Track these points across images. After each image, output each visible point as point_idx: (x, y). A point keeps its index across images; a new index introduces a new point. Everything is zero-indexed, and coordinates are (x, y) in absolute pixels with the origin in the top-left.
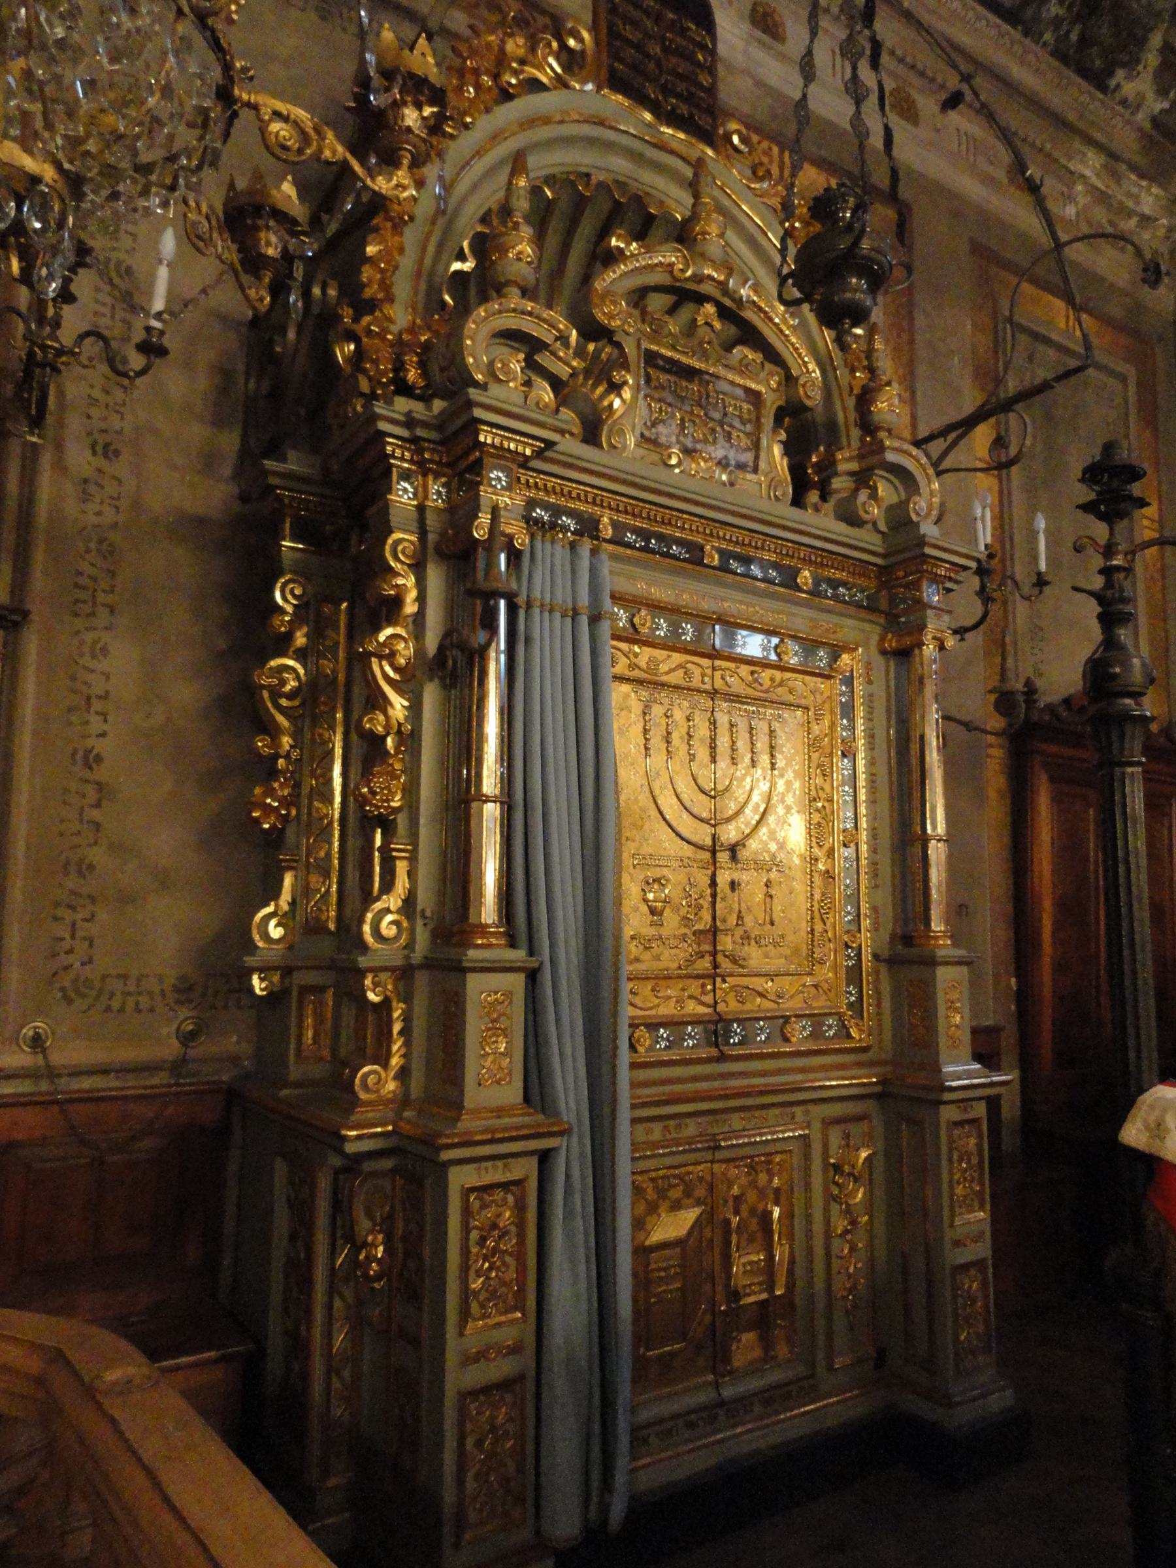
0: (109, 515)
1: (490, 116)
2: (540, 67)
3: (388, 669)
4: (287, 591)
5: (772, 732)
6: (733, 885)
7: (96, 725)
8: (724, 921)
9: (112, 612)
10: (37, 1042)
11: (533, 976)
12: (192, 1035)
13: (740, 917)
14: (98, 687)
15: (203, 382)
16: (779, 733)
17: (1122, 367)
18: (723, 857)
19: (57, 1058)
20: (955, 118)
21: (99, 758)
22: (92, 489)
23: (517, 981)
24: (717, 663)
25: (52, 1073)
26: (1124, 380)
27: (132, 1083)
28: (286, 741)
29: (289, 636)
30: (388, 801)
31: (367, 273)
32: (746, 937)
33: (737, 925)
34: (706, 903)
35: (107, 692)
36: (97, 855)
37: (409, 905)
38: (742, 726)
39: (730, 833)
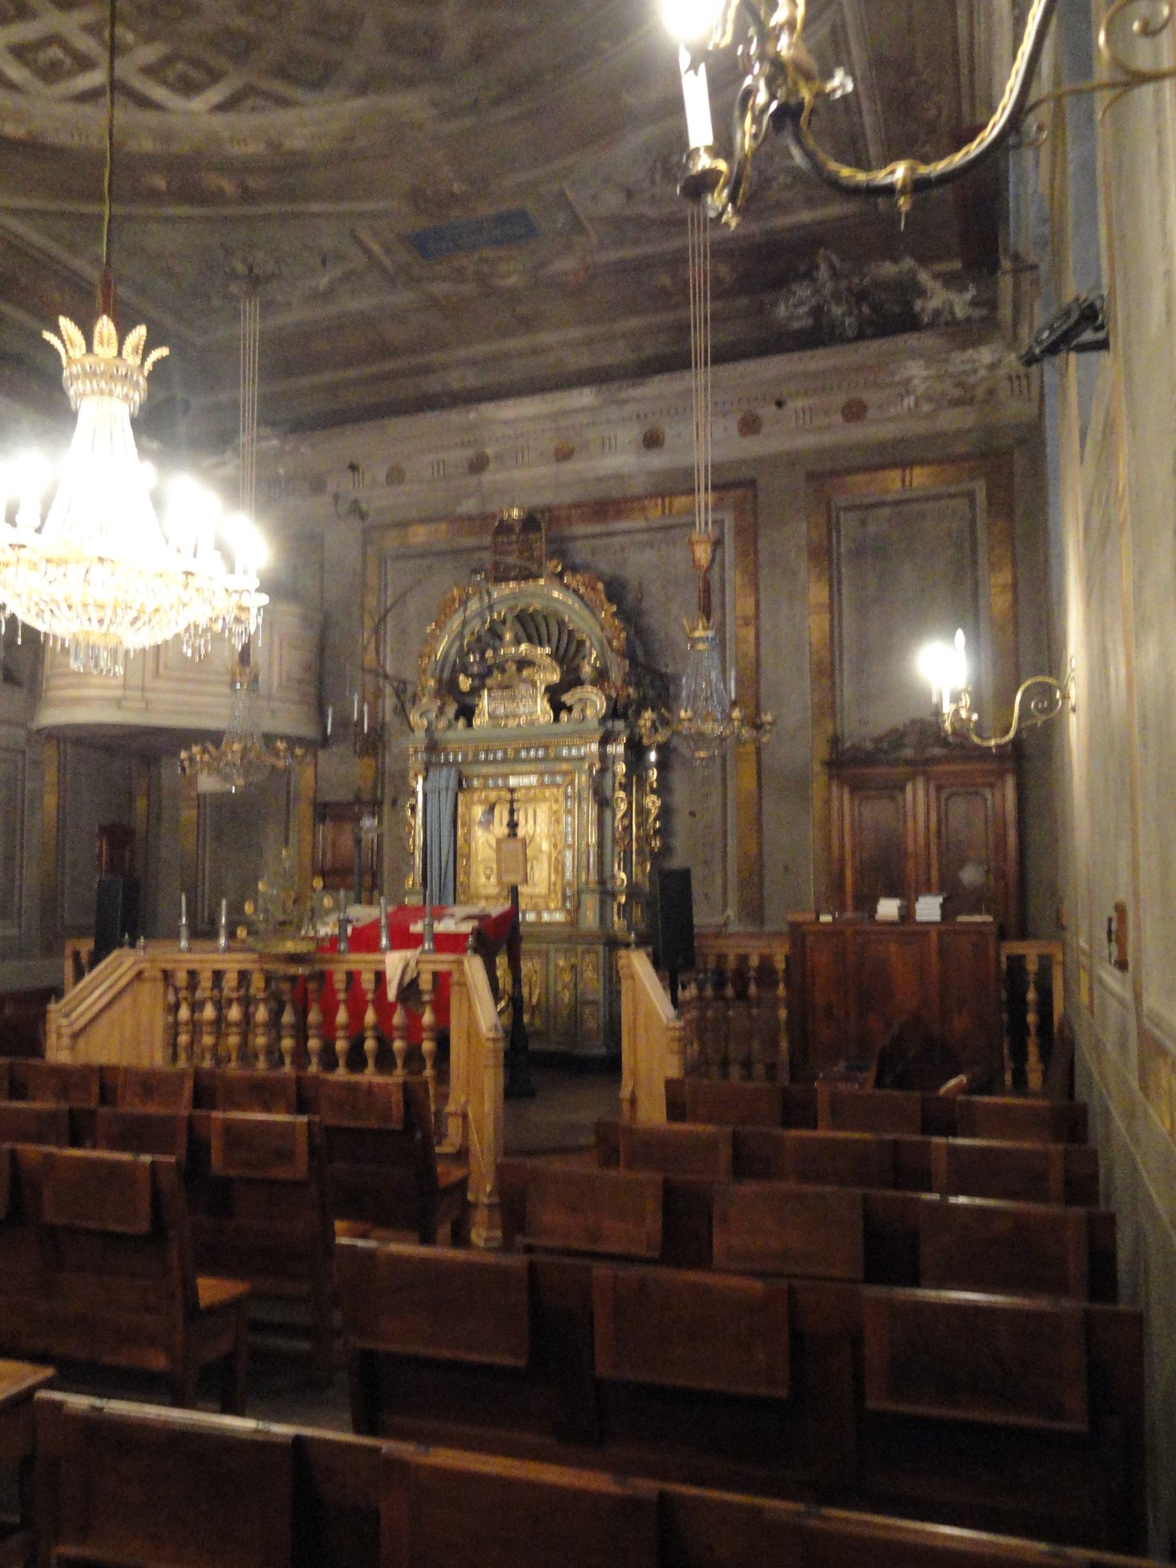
17: (965, 486)
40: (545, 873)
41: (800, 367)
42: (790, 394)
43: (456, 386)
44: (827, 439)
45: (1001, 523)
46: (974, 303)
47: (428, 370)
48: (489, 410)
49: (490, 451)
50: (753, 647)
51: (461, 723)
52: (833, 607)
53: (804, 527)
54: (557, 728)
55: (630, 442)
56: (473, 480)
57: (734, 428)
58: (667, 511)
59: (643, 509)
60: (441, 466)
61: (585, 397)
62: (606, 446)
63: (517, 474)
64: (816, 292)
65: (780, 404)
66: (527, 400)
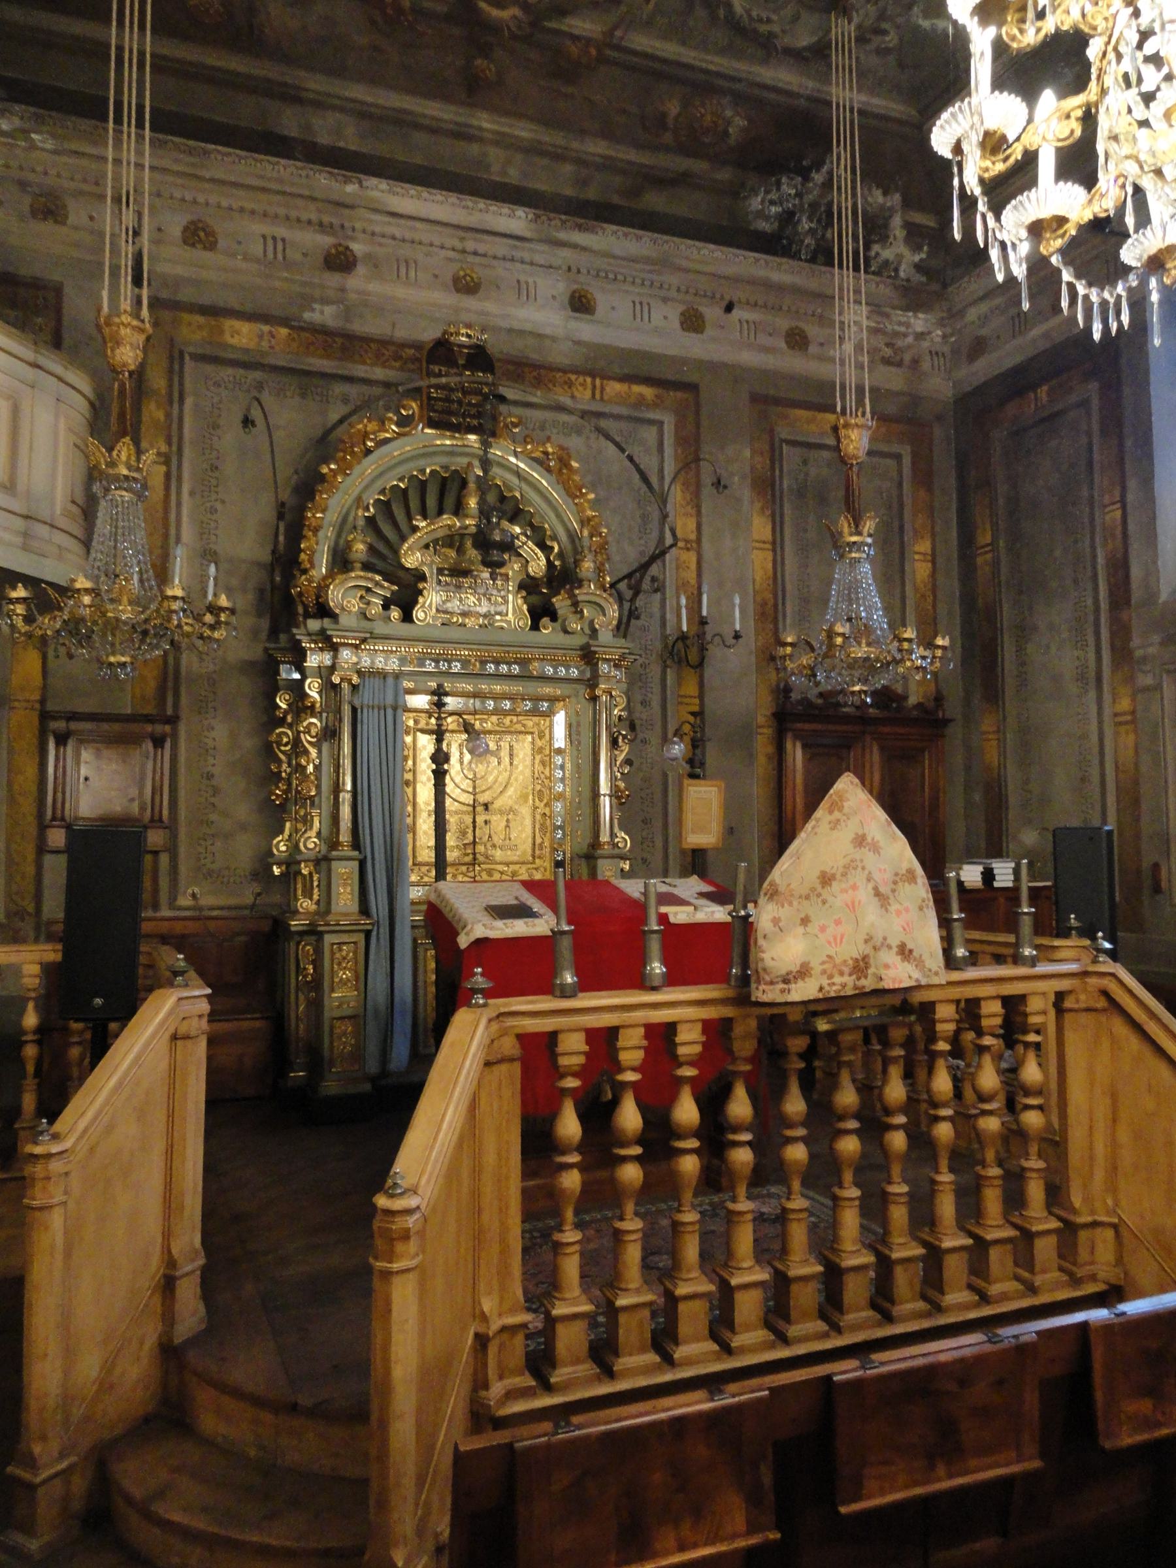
0: (211, 667)
2: (387, 431)
3: (309, 738)
5: (511, 747)
6: (486, 822)
7: (211, 761)
10: (194, 895)
12: (259, 894)
13: (490, 836)
14: (211, 743)
15: (250, 596)
17: (895, 448)
18: (479, 809)
19: (203, 902)
20: (737, 313)
21: (213, 776)
22: (204, 657)
23: (356, 864)
25: (201, 909)
26: (898, 457)
27: (234, 913)
28: (285, 766)
29: (284, 718)
31: (303, 556)
32: (494, 846)
34: (470, 831)
36: (213, 817)
37: (319, 835)
39: (483, 798)
41: (761, 272)
43: (324, 139)
44: (770, 362)
45: (922, 493)
46: (918, 267)
47: (293, 96)
48: (378, 189)
49: (357, 248)
50: (694, 575)
51: (395, 613)
52: (776, 545)
53: (747, 453)
54: (534, 637)
56: (333, 280)
58: (598, 396)
59: (570, 384)
61: (516, 220)
62: (523, 292)
63: (401, 292)
64: (799, 195)
65: (729, 308)
66: (439, 196)
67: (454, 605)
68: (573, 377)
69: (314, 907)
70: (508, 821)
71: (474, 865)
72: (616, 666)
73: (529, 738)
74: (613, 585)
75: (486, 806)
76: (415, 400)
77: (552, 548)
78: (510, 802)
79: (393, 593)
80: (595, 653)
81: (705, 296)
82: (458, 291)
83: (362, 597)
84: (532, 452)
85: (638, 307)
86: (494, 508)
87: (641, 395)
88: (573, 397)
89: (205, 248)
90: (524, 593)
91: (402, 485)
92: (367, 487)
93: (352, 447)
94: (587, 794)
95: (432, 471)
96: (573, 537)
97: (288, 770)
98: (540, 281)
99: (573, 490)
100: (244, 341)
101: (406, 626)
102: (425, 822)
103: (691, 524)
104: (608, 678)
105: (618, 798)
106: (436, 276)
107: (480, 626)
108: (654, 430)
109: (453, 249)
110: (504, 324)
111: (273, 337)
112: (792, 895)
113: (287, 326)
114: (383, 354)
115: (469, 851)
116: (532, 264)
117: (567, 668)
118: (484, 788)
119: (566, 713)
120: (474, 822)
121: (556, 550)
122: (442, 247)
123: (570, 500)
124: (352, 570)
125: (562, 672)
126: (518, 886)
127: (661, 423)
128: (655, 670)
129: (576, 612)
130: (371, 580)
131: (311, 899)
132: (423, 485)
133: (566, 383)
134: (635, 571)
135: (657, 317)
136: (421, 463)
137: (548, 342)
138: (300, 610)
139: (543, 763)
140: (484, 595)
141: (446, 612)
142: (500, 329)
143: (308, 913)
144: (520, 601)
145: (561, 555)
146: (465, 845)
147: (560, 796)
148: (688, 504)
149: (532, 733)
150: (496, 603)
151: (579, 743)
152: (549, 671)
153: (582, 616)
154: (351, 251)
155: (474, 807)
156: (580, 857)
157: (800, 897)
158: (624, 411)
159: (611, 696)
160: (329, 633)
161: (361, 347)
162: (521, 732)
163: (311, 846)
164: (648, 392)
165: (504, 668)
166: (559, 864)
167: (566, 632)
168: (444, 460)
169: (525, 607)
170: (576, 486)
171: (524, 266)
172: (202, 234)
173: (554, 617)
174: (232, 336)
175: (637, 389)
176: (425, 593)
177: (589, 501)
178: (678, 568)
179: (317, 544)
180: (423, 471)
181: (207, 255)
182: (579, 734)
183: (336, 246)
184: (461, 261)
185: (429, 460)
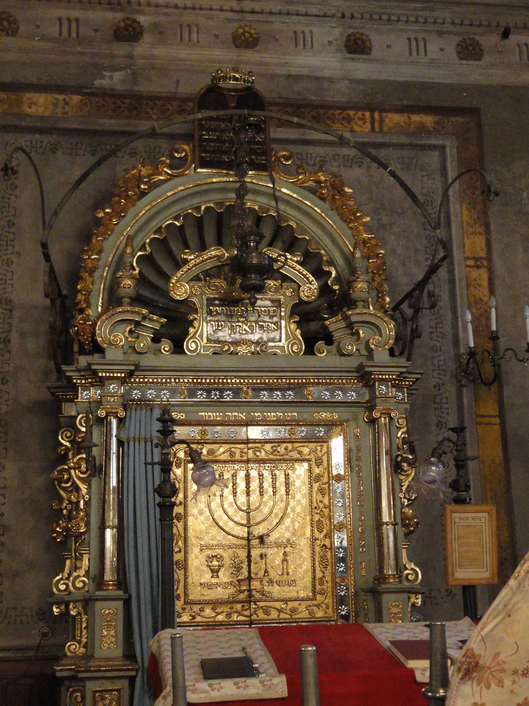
1: (134, 208)
2: (161, 174)
4: (64, 435)
5: (287, 476)
6: (262, 556)
8: (256, 574)
9: (6, 450)
11: (127, 603)
13: (266, 571)
16: (291, 475)
18: (255, 542)
20: (514, 38)
23: (120, 604)
24: (250, 445)
27: (19, 654)
30: (79, 529)
32: (271, 582)
33: (264, 575)
34: (245, 566)
35: (5, 486)
38: (266, 473)
40: (307, 565)
42: (516, 27)
49: (143, 19)
51: (166, 346)
54: (311, 361)
55: (330, 43)
57: (451, 52)
59: (349, 120)
60: (74, 25)
65: (506, 34)
67: (225, 334)
68: (352, 113)
69: (82, 650)
70: (285, 554)
71: (250, 602)
72: (398, 388)
73: (306, 465)
74: (395, 308)
75: (262, 539)
76: (188, 145)
77: (330, 273)
78: (287, 535)
79: (162, 326)
80: (370, 373)
81: (480, 25)
82: (237, 47)
83: (131, 332)
84: (304, 182)
85: (414, 43)
86: (251, 233)
87: (421, 123)
88: (352, 131)
89: (7, 35)
90: (297, 319)
91: (178, 224)
92: (141, 228)
93: (127, 190)
94: (371, 523)
95: (206, 208)
96: (349, 260)
97: (69, 507)
98: (315, 30)
99: (348, 215)
100: (40, 110)
101: (178, 358)
102: (197, 557)
103: (480, 242)
104: (385, 397)
105: (407, 526)
106: (217, 36)
107: (253, 353)
108: (436, 153)
109: (232, 11)
110: (283, 71)
111: (67, 104)
112: (503, 670)
113: (77, 93)
114: (168, 110)
115: (244, 588)
116: (306, 15)
117: (345, 392)
118: (259, 519)
119: (345, 438)
120: (249, 556)
121: (334, 274)
122: (221, 10)
123: (344, 225)
124: (120, 304)
125: (339, 396)
126: (253, 633)
127: (444, 147)
128: (451, 389)
129: (352, 334)
130: (138, 313)
131: (79, 642)
132: (199, 222)
133: (344, 119)
134: (414, 290)
135: (433, 47)
136: (195, 201)
137: (325, 84)
138: (76, 348)
139: (321, 491)
140: (256, 322)
141: (218, 341)
142: (279, 76)
143: (76, 657)
144: (293, 326)
145: (338, 279)
146: (239, 581)
147: (340, 527)
148: (475, 222)
149: (309, 460)
150: (269, 330)
151: (360, 467)
152: (326, 395)
153: (359, 338)
154: (139, 23)
155: (249, 540)
156: (365, 591)
157: (515, 672)
158: (403, 140)
159: (391, 419)
160: (93, 367)
161: (148, 104)
162: (297, 460)
163: (80, 585)
164: (428, 120)
165: (278, 396)
166: (341, 601)
167: (342, 355)
168: (218, 197)
169: (298, 332)
170: (350, 211)
171: (299, 18)
172: (5, 23)
173: (329, 340)
174: (30, 107)
175: (415, 118)
176: (196, 324)
177: (365, 224)
178: (468, 286)
179: (93, 283)
180: (198, 209)
181: (9, 41)
182: (359, 459)
183: (124, 20)
184: (240, 20)
185: (204, 198)
